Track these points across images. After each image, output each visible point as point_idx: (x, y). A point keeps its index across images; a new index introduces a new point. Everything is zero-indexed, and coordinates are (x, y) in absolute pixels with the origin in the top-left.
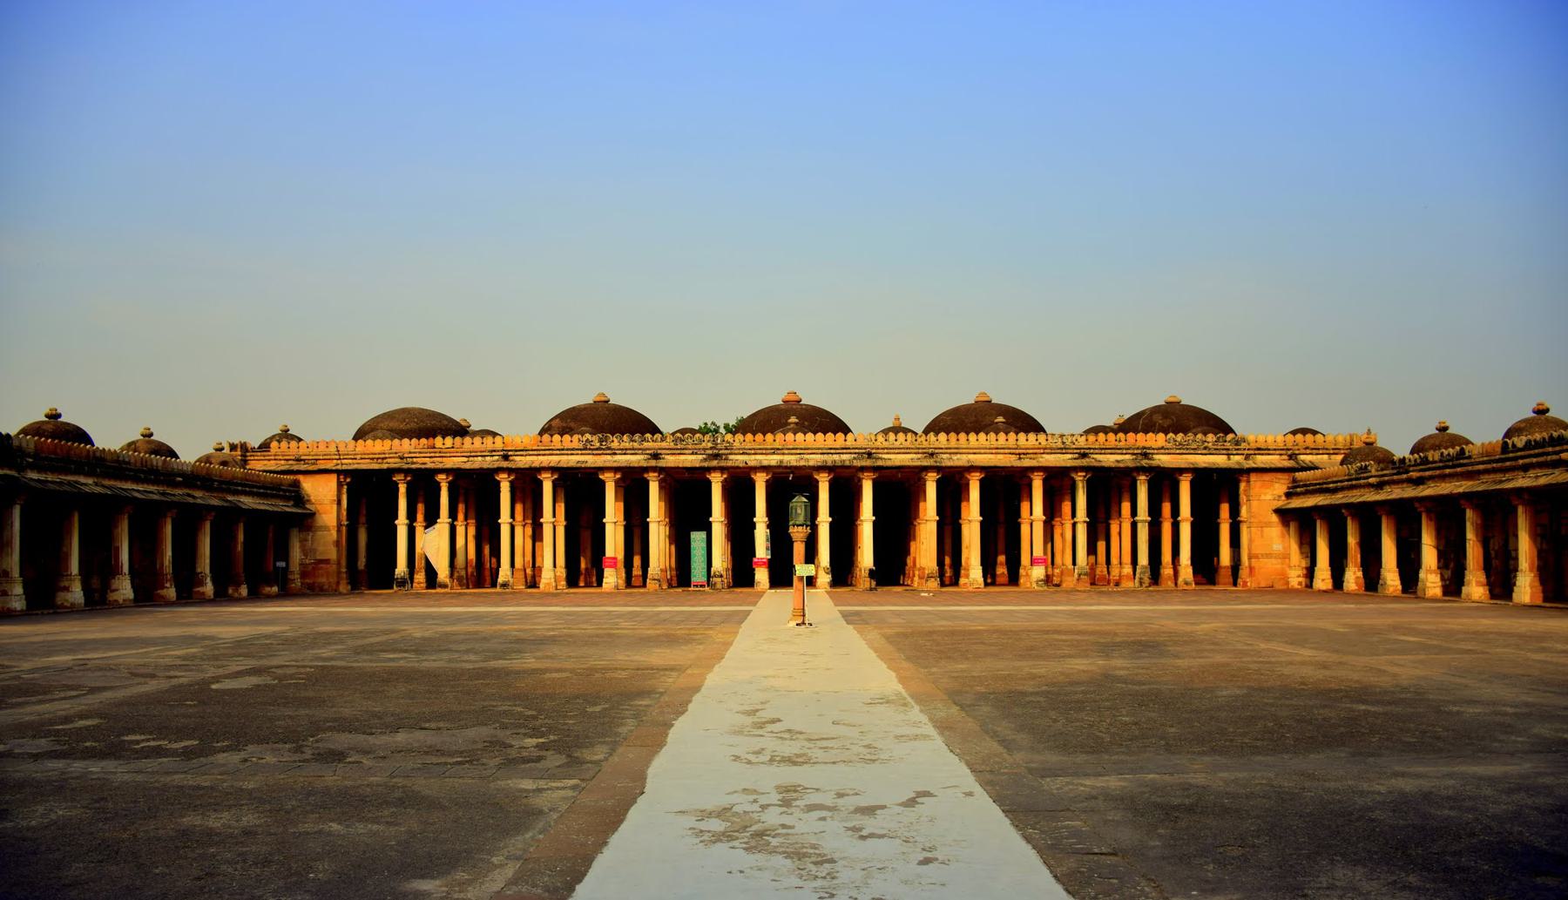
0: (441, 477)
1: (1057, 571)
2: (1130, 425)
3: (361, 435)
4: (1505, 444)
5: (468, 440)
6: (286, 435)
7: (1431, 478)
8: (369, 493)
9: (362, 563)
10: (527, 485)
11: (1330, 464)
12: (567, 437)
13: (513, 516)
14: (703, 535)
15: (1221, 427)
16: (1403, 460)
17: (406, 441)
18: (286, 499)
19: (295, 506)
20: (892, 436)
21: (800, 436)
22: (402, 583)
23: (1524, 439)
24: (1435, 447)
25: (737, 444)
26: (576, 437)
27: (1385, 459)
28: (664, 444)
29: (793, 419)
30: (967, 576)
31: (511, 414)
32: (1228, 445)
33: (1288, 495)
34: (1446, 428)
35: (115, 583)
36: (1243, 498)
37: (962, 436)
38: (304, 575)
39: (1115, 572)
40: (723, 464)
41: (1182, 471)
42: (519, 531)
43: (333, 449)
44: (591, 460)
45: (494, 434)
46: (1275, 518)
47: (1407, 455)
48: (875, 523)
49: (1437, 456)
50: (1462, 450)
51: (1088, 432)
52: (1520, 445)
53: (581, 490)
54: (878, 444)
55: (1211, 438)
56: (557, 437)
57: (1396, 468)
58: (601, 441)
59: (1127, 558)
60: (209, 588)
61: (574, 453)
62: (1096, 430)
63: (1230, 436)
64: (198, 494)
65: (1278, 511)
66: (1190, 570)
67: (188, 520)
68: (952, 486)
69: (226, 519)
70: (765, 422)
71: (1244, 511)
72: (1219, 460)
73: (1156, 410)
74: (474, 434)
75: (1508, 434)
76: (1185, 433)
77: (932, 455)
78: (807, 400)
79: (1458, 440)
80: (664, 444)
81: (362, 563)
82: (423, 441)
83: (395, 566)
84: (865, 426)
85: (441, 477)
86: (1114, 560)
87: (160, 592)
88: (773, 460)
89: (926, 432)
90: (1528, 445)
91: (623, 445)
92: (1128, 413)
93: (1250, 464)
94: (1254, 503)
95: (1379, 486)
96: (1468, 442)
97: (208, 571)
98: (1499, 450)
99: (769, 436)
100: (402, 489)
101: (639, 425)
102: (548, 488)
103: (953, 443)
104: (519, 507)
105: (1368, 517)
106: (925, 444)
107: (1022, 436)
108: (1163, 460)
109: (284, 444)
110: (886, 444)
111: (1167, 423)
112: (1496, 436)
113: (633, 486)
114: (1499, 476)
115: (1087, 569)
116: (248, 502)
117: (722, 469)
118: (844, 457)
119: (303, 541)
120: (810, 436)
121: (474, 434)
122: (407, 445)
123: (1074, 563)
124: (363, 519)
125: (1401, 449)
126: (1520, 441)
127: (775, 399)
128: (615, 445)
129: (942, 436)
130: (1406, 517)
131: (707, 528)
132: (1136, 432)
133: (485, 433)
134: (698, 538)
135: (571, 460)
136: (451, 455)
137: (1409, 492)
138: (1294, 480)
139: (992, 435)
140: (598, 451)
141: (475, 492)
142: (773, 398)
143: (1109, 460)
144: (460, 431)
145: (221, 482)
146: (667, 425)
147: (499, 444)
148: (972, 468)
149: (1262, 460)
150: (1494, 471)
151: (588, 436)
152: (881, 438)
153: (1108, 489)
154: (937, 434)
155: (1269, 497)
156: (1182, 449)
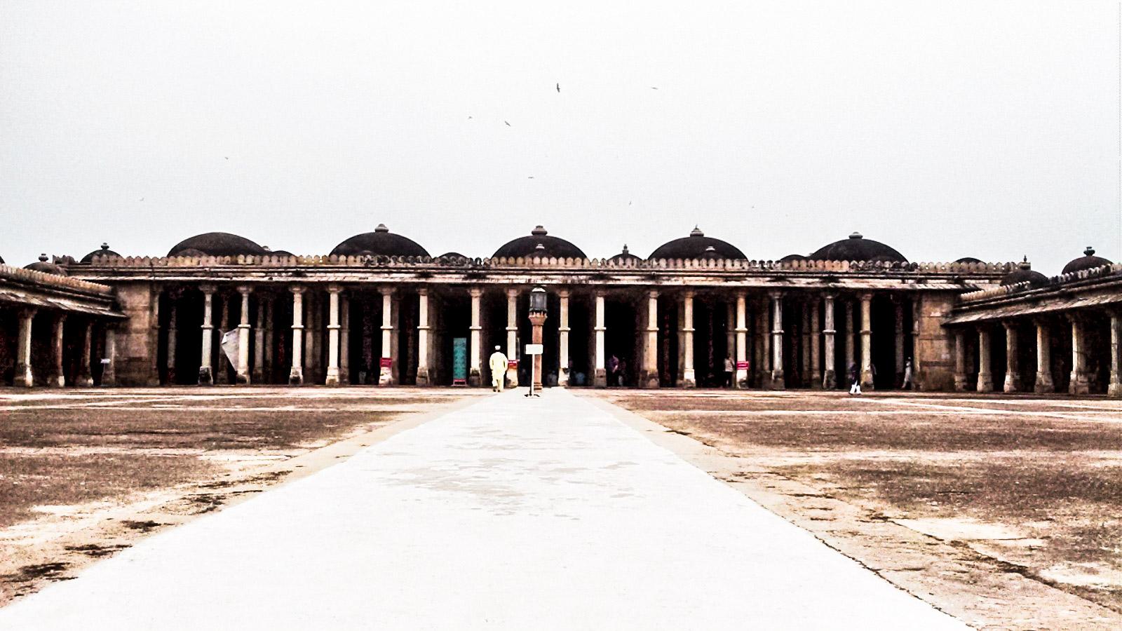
0: (242, 289)
2: (823, 254)
3: (175, 252)
7: (1080, 293)
9: (171, 362)
10: (317, 297)
12: (351, 258)
14: (464, 340)
17: (212, 258)
18: (105, 305)
19: (112, 310)
21: (545, 260)
24: (1086, 267)
25: (493, 266)
27: (1039, 280)
28: (432, 265)
32: (902, 271)
43: (147, 264)
45: (289, 255)
47: (1060, 275)
49: (1085, 273)
50: (1108, 268)
53: (362, 304)
56: (343, 258)
58: (379, 261)
60: (29, 378)
63: (904, 264)
64: (21, 295)
65: (944, 326)
66: (870, 376)
68: (670, 303)
69: (47, 318)
70: (516, 250)
74: (271, 254)
79: (1100, 262)
80: (432, 265)
81: (171, 362)
82: (228, 258)
83: (200, 364)
84: (598, 250)
85: (242, 289)
94: (925, 320)
97: (28, 361)
99: (520, 260)
101: (407, 249)
102: (334, 299)
104: (309, 336)
105: (1025, 327)
106: (649, 268)
108: (850, 284)
110: (616, 268)
113: (406, 299)
116: (68, 304)
117: (480, 286)
118: (582, 277)
119: (118, 342)
120: (553, 261)
122: (212, 262)
123: (771, 367)
124: (173, 324)
125: (1052, 269)
128: (392, 264)
129: (663, 262)
130: (1057, 326)
131: (468, 335)
133: (281, 254)
134: (459, 343)
137: (1061, 306)
139: (704, 261)
141: (271, 305)
142: (525, 231)
143: (802, 283)
144: (259, 251)
145: (42, 286)
146: (435, 251)
147: (293, 263)
148: (687, 288)
149: (932, 284)
151: (369, 257)
152: (612, 263)
153: (801, 307)
155: (938, 314)
156: (859, 273)
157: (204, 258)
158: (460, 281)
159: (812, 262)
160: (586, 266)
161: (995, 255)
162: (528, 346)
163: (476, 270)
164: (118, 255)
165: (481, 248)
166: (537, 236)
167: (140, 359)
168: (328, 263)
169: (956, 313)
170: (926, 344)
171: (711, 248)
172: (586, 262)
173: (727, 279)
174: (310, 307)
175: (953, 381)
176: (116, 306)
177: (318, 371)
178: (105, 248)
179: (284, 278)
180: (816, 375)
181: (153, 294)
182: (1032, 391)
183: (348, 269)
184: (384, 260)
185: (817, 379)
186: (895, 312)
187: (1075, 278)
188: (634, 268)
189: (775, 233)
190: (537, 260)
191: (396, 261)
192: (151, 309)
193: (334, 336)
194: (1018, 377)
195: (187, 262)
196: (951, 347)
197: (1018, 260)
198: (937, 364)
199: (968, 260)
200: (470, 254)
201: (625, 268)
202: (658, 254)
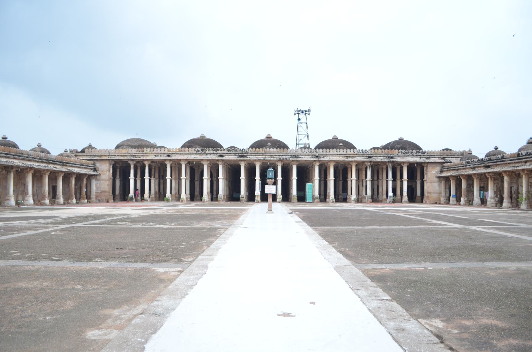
1: (360, 197)
2: (385, 147)
3: (118, 147)
4: (519, 154)
5: (155, 149)
6: (90, 147)
8: (121, 169)
10: (176, 166)
11: (456, 161)
12: (190, 149)
13: (171, 176)
15: (418, 148)
16: (482, 159)
17: (133, 149)
20: (303, 150)
21: (271, 149)
22: (131, 199)
23: (525, 152)
24: (494, 155)
25: (250, 152)
26: (193, 149)
28: (224, 152)
29: (269, 144)
30: (329, 199)
31: (171, 141)
32: (420, 154)
33: (441, 172)
34: (6, 138)
35: (26, 198)
36: (425, 172)
37: (328, 150)
38: (97, 196)
39: (380, 198)
40: (245, 159)
41: (404, 163)
42: (173, 182)
43: (107, 152)
44: (199, 157)
45: (165, 148)
46: (436, 179)
48: (297, 180)
50: (503, 156)
51: (371, 149)
52: (524, 154)
54: (298, 153)
55: (414, 151)
56: (187, 149)
57: (21, 155)
58: (202, 150)
59: (384, 193)
61: (193, 155)
62: (374, 148)
63: (421, 151)
66: (407, 197)
67: (53, 176)
70: (258, 145)
71: (425, 177)
72: (417, 160)
73: (395, 142)
74: (157, 148)
75: (520, 150)
76: (405, 149)
77: (317, 157)
78: (274, 137)
80: (224, 152)
83: (129, 193)
85: (145, 162)
86: (380, 194)
87: (43, 201)
88: (262, 158)
89: (315, 148)
90: (527, 154)
91: (210, 152)
92: (384, 144)
93: (428, 161)
95: (474, 168)
96: (505, 153)
98: (516, 155)
99: (261, 149)
100: (132, 166)
101: (212, 145)
103: (325, 153)
106: (315, 153)
107: (348, 150)
108: (399, 159)
109: (90, 150)
110: (301, 153)
111: (399, 146)
112: (515, 151)
114: (517, 165)
115: (371, 197)
117: (244, 160)
118: (287, 157)
120: (275, 150)
121: (157, 148)
122: (134, 151)
123: (366, 194)
126: (524, 153)
127: (263, 137)
128: (207, 152)
129: (321, 150)
130: (483, 178)
132: (388, 149)
133: (161, 147)
135: (191, 157)
136: (149, 156)
138: (443, 167)
139: (338, 150)
140: (201, 154)
141: (159, 169)
143: (379, 159)
146: (225, 146)
147: (166, 151)
149: (432, 160)
150: (515, 163)
151: (198, 148)
152: (299, 151)
153: (377, 169)
154: (319, 149)
155: (434, 172)
156: (405, 155)
157: (130, 150)
158: (236, 159)
159: (383, 150)
160: (288, 152)
161: (457, 148)
162: (266, 186)
163: (242, 154)
164: (96, 149)
165: (244, 144)
166: (268, 139)
167: (105, 191)
168: (179, 152)
169: (441, 172)
170: (429, 184)
171: (341, 144)
172: (289, 150)
173: (348, 157)
174: (173, 169)
175: (440, 200)
176: (95, 170)
177: (177, 195)
178: (90, 146)
179: (163, 158)
180: (385, 197)
181: (110, 164)
182: (472, 204)
183: (189, 154)
184: (204, 150)
185: (385, 199)
186: (416, 171)
187: (490, 160)
188: (309, 153)
189: (368, 137)
190: (268, 149)
191: (209, 150)
192: (109, 171)
193: (183, 182)
194: (466, 199)
195: (124, 151)
196: (440, 185)
197: (467, 150)
198: (434, 193)
199: (447, 149)
200: (241, 147)
201: (305, 153)
202: (319, 147)
